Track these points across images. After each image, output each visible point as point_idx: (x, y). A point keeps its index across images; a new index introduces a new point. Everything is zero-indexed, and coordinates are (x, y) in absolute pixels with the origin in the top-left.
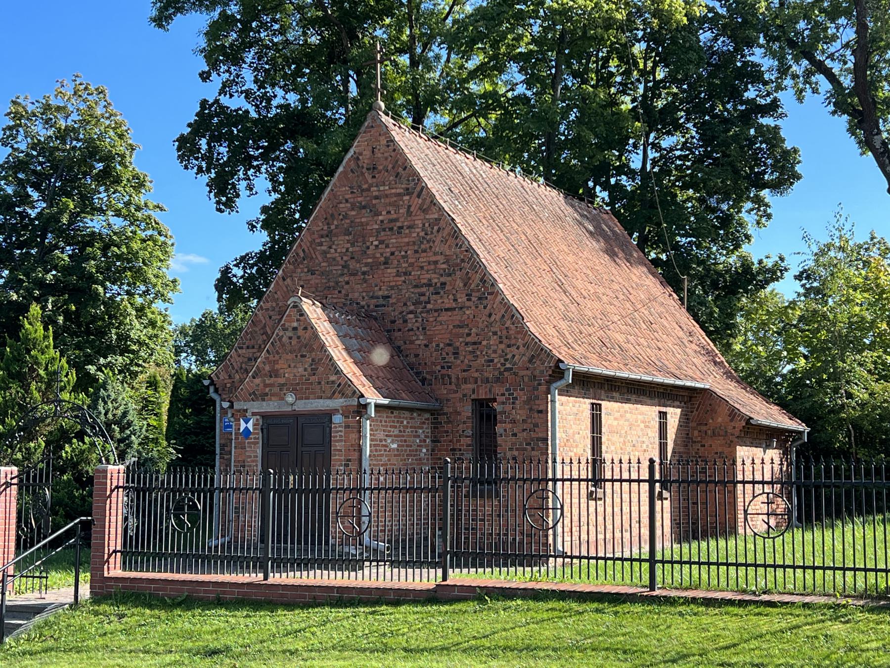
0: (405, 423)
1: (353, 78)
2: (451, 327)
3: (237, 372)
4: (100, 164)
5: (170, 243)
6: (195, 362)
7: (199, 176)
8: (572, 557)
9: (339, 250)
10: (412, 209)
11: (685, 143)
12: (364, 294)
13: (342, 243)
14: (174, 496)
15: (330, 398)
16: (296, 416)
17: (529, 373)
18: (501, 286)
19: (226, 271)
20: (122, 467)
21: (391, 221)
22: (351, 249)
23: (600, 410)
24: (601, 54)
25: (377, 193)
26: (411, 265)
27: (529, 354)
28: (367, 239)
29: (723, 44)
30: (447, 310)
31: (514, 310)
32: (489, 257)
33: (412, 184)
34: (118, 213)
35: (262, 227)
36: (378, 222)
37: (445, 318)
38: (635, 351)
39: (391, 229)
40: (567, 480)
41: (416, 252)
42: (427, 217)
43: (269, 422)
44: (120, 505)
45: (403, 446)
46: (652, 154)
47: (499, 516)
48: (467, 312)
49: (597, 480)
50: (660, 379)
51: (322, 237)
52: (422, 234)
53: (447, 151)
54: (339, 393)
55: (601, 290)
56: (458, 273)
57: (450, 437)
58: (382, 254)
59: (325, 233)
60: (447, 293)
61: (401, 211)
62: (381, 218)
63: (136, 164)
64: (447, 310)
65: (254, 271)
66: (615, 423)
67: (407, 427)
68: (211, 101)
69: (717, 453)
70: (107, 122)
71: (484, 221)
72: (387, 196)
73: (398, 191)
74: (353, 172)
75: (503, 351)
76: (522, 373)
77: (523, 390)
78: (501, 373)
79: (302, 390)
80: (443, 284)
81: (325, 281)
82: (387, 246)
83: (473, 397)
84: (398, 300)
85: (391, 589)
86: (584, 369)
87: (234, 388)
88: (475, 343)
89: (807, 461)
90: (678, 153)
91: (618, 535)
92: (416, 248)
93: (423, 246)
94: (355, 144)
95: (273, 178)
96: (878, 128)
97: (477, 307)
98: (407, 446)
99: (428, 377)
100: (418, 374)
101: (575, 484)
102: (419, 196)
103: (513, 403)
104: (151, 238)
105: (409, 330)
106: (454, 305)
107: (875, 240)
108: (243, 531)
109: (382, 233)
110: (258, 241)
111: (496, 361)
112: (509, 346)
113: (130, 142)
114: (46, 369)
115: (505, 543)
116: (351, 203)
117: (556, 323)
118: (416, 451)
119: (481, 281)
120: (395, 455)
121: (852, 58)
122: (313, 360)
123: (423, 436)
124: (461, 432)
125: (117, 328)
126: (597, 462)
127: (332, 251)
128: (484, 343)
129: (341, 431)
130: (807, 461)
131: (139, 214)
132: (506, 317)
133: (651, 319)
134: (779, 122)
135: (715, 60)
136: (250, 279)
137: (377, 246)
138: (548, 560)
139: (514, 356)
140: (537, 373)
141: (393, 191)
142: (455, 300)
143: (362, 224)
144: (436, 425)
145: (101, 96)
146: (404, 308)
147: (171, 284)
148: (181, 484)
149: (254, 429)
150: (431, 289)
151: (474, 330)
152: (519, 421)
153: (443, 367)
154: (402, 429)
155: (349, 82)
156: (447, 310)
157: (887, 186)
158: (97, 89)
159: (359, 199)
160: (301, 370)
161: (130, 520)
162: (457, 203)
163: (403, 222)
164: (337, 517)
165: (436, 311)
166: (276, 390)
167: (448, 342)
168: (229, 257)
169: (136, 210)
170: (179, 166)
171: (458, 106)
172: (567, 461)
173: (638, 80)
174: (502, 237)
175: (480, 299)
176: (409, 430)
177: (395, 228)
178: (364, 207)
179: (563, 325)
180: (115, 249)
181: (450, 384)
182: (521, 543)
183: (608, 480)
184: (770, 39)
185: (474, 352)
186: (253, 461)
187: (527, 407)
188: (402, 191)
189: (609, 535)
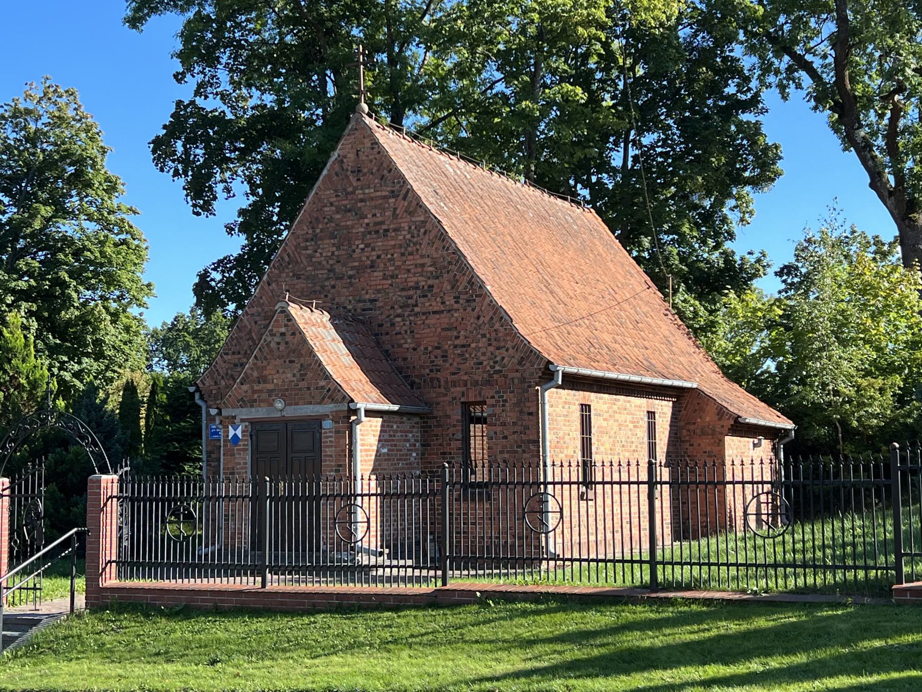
0: (395, 427)
1: (330, 77)
2: (439, 330)
3: (223, 378)
4: (72, 168)
5: (144, 246)
7: (176, 178)
8: (564, 560)
9: (324, 254)
10: (398, 212)
11: (664, 141)
12: (351, 298)
13: (327, 247)
14: (169, 506)
15: (320, 403)
16: (286, 422)
17: (518, 375)
18: (489, 287)
19: (204, 276)
20: (116, 477)
21: (376, 224)
22: (336, 253)
23: (590, 411)
24: (579, 51)
25: (362, 196)
26: (398, 267)
27: (518, 356)
29: (703, 40)
30: (435, 313)
32: (476, 259)
33: (397, 187)
34: (90, 218)
35: (240, 231)
36: (364, 225)
37: (433, 322)
38: (622, 351)
39: (377, 232)
40: (558, 483)
41: (403, 254)
42: (414, 219)
43: (257, 428)
44: (114, 515)
45: (393, 450)
46: (633, 152)
47: (491, 519)
49: (588, 482)
50: (647, 380)
51: (307, 241)
52: (409, 236)
55: (588, 289)
56: (445, 275)
57: (440, 441)
58: (368, 258)
60: (435, 296)
62: (366, 221)
63: (109, 166)
64: (435, 313)
65: (232, 275)
66: (604, 424)
67: (396, 431)
68: (186, 102)
69: (705, 452)
70: (78, 125)
71: (471, 224)
72: (372, 199)
73: (384, 193)
75: (492, 354)
76: (511, 375)
77: (512, 392)
78: (490, 376)
79: (290, 395)
80: (431, 287)
81: (310, 285)
82: (373, 249)
83: (462, 400)
85: (391, 595)
86: (574, 370)
88: (463, 346)
89: (796, 461)
90: (659, 150)
91: (609, 536)
92: (403, 250)
93: (409, 249)
94: (339, 147)
95: (250, 180)
96: (859, 121)
97: (465, 310)
98: (397, 450)
99: (417, 380)
100: (406, 377)
101: (566, 487)
102: (404, 199)
103: (503, 406)
104: (124, 242)
105: (396, 334)
106: (442, 309)
107: (856, 234)
108: (233, 538)
109: (368, 236)
110: (236, 245)
111: (485, 363)
112: (498, 348)
113: (101, 144)
114: (27, 377)
115: (497, 546)
116: (337, 207)
117: (543, 324)
118: (407, 455)
119: (469, 283)
120: (386, 460)
121: (832, 52)
122: (302, 365)
124: (451, 435)
125: (93, 333)
126: (587, 465)
127: (318, 255)
128: (473, 345)
129: (331, 437)
130: (796, 461)
131: (112, 218)
132: (495, 319)
133: (637, 318)
134: (760, 118)
135: (695, 55)
136: (229, 282)
137: (362, 249)
138: (541, 563)
139: (503, 358)
140: (527, 375)
141: (378, 194)
142: (443, 303)
143: (347, 227)
144: (425, 429)
145: (72, 97)
146: (392, 312)
147: (146, 289)
149: (243, 436)
150: (419, 292)
151: (462, 333)
152: (509, 424)
153: (431, 371)
155: (326, 82)
156: (435, 313)
157: (869, 181)
158: (67, 92)
159: (344, 202)
160: (289, 375)
161: (125, 531)
162: (442, 204)
163: (389, 225)
164: (335, 523)
165: (424, 314)
166: (264, 396)
168: (207, 260)
169: (109, 214)
170: (155, 171)
171: (436, 105)
172: (558, 463)
173: (618, 77)
174: (488, 238)
175: (468, 301)
176: (399, 434)
178: (349, 211)
179: (551, 325)
180: (88, 254)
182: (513, 546)
183: (599, 483)
184: (750, 35)
185: (463, 355)
186: (242, 468)
188: (387, 193)
189: (601, 537)
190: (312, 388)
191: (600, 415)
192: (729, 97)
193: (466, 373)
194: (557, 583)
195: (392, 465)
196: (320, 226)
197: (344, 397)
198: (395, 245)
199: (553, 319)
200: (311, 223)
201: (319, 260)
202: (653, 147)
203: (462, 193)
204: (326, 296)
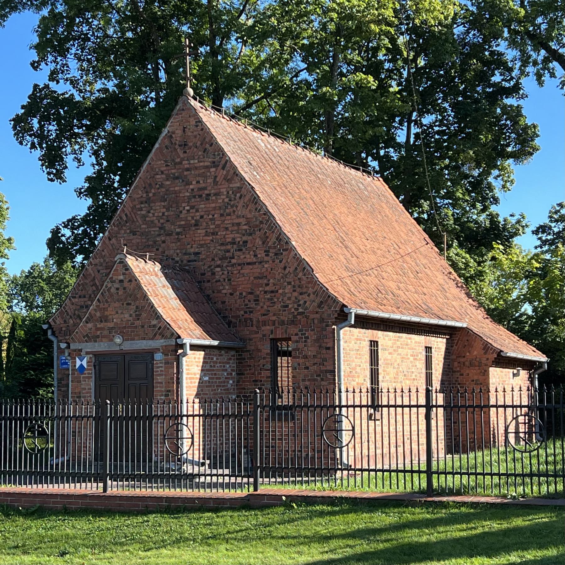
0: (215, 359)
1: (162, 66)
2: (252, 278)
3: (71, 317)
5: (5, 207)
6: (25, 307)
9: (156, 214)
10: (218, 180)
12: (178, 251)
13: (159, 208)
15: (152, 339)
16: (123, 355)
17: (318, 316)
18: (294, 243)
19: (56, 232)
22: (166, 214)
23: (377, 347)
26: (218, 226)
28: (179, 205)
29: (474, 37)
31: (305, 263)
36: (189, 190)
38: (405, 297)
41: (222, 215)
45: (213, 378)
46: (415, 130)
48: (266, 266)
51: (142, 203)
52: (227, 200)
53: (245, 129)
54: (160, 335)
55: (377, 245)
56: (258, 233)
57: (252, 371)
58: (193, 218)
59: (144, 199)
61: (208, 181)
62: (191, 187)
64: (249, 264)
66: (389, 357)
69: (473, 381)
71: (279, 189)
72: (196, 168)
74: (167, 148)
75: (296, 299)
76: (312, 316)
77: (313, 330)
78: (295, 317)
82: (197, 211)
83: (271, 337)
84: (208, 256)
87: (69, 332)
88: (272, 292)
90: (436, 129)
91: (393, 450)
92: (222, 212)
94: (169, 124)
98: (217, 378)
99: (233, 320)
102: (223, 168)
105: (216, 281)
109: (193, 200)
111: (290, 306)
118: (224, 382)
122: (137, 307)
123: (229, 370)
124: (261, 366)
127: (151, 215)
129: (161, 367)
134: (521, 102)
137: (188, 211)
139: (305, 302)
140: (325, 315)
141: (202, 164)
142: (255, 256)
143: (175, 192)
144: (240, 361)
146: (212, 263)
148: (31, 414)
149: (88, 366)
150: (235, 246)
151: (271, 281)
153: (245, 312)
154: (212, 364)
159: (173, 171)
160: (127, 316)
164: (164, 439)
165: (239, 265)
166: (106, 332)
167: (250, 291)
177: (204, 195)
178: (177, 178)
181: (252, 326)
182: (313, 458)
187: (317, 345)
188: (209, 164)
190: (146, 326)
191: (386, 350)
192: (495, 85)
193: (274, 315)
194: (350, 489)
195: (212, 390)
196: (153, 191)
197: (173, 334)
198: (215, 207)
199: (348, 269)
200: (145, 188)
201: (152, 219)
202: (431, 126)
203: (271, 164)
204: (157, 250)
